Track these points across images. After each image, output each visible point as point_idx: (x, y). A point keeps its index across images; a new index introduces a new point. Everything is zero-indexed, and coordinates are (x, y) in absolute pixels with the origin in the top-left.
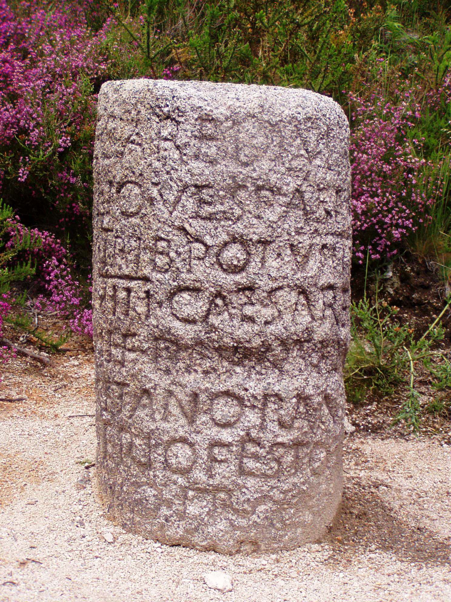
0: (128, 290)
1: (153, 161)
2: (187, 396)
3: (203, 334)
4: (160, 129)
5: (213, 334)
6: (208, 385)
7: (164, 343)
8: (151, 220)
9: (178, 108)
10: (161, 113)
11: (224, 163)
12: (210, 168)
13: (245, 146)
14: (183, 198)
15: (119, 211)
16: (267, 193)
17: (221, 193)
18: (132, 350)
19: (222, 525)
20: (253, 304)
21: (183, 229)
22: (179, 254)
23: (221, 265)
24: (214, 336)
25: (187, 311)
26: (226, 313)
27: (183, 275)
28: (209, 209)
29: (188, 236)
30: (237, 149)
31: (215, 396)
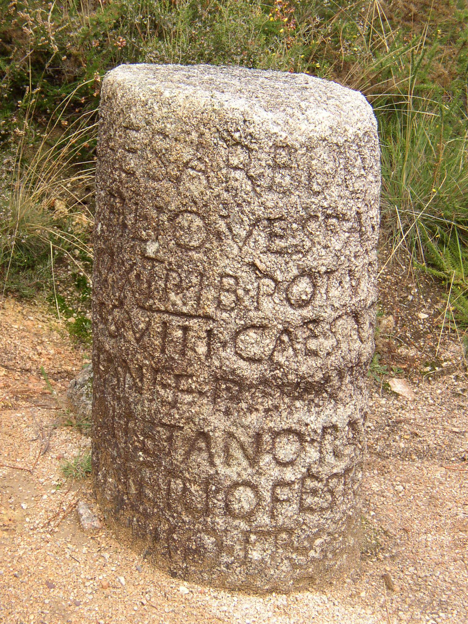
0: (185, 329)
1: (221, 192)
2: (250, 437)
3: (268, 372)
4: (228, 156)
5: (278, 371)
6: (271, 425)
7: (225, 384)
8: (218, 255)
9: (250, 134)
10: (229, 138)
11: (297, 193)
12: (285, 200)
13: (317, 174)
14: (255, 232)
15: (173, 242)
16: (334, 220)
17: (295, 226)
18: (189, 391)
19: (285, 566)
20: (316, 337)
21: (253, 265)
22: (247, 291)
23: (288, 300)
24: (279, 373)
25: (255, 351)
26: (291, 349)
27: (251, 314)
28: (280, 244)
29: (257, 272)
30: (310, 178)
31: (276, 434)
